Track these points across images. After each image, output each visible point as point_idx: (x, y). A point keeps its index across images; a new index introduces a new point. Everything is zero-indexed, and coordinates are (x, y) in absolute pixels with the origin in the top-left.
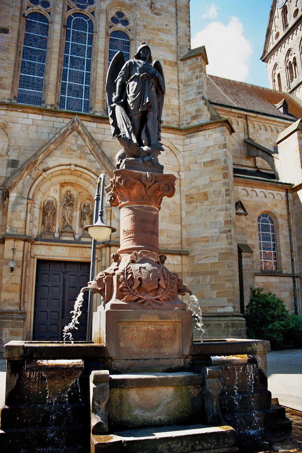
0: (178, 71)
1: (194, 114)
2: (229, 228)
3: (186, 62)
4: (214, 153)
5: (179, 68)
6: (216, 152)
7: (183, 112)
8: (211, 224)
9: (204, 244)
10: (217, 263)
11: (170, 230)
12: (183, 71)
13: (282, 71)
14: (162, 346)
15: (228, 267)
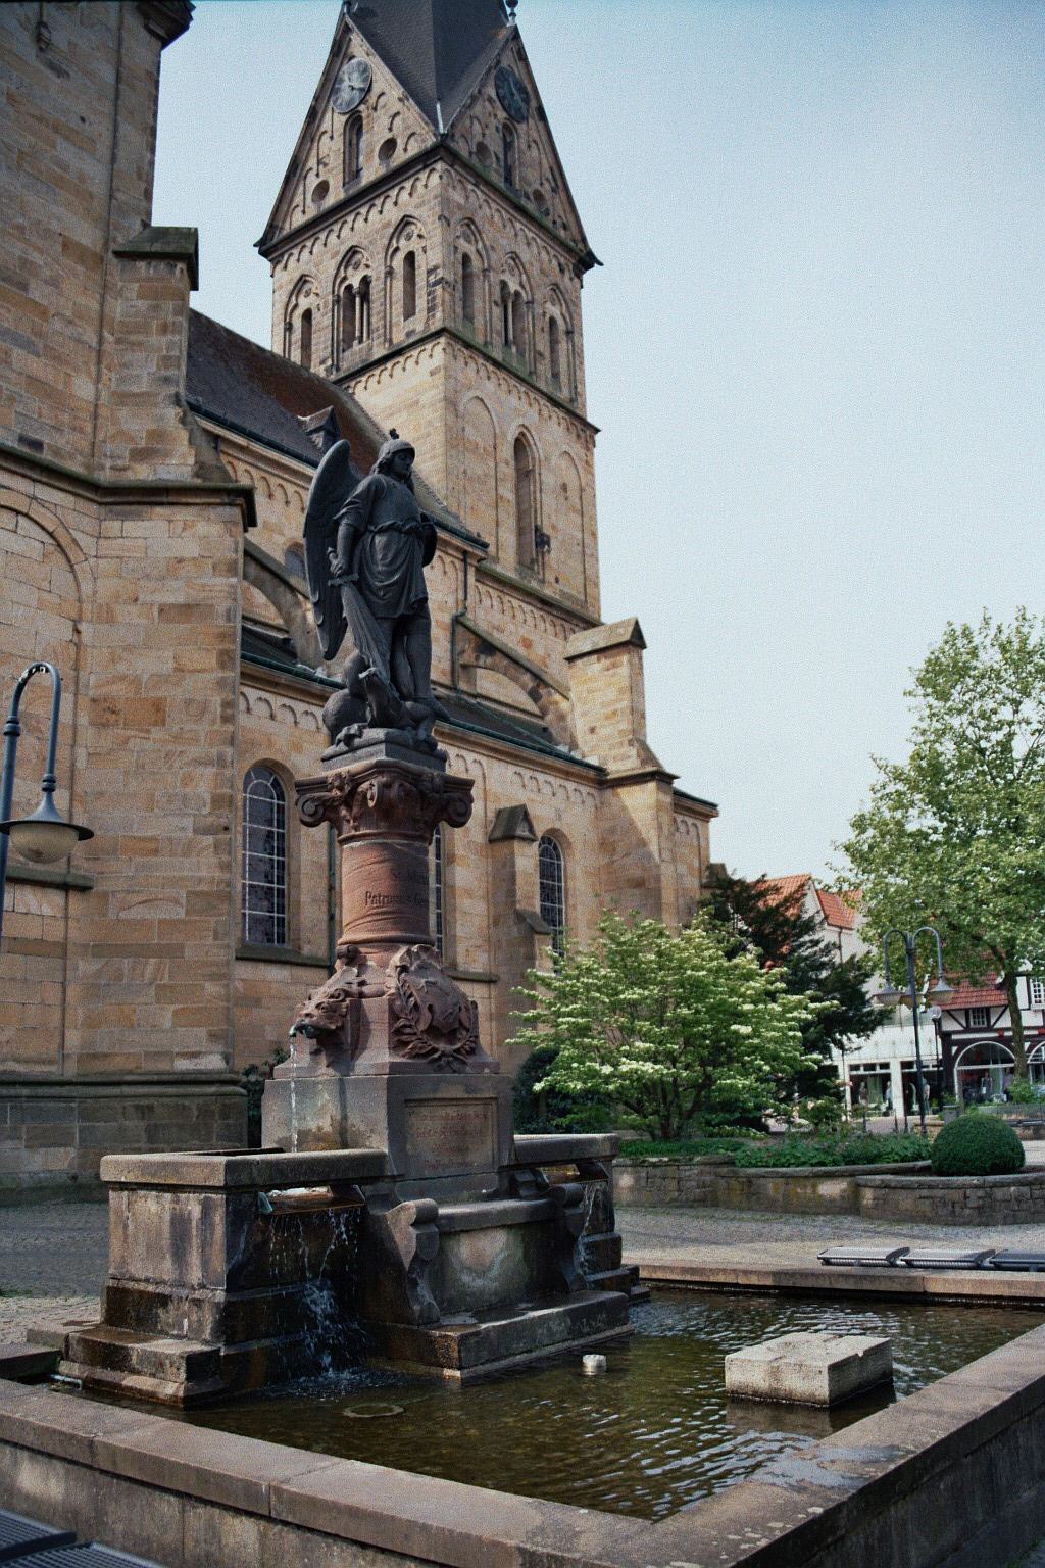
0: (105, 286)
1: (142, 444)
2: (224, 821)
3: (132, 263)
4: (198, 581)
5: (109, 277)
6: (205, 580)
7: (106, 430)
8: (170, 802)
9: (139, 859)
10: (179, 921)
12: (120, 293)
13: (322, 307)
15: (216, 938)
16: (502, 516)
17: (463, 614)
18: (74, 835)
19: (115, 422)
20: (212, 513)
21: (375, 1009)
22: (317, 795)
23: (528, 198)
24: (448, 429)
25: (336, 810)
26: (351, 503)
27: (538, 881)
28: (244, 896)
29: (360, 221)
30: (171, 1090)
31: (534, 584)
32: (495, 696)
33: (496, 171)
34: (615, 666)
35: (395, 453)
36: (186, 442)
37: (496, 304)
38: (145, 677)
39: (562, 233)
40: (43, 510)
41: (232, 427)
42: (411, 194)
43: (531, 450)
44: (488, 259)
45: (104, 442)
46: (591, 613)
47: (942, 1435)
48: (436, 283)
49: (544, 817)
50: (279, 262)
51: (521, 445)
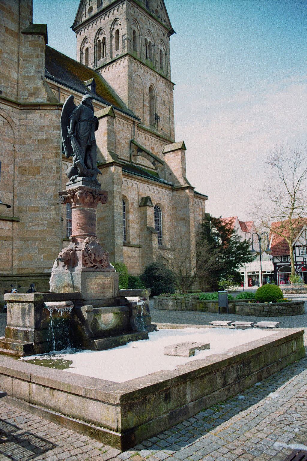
1: (32, 91)
6: (51, 132)
7: (21, 87)
8: (42, 196)
11: (3, 197)
13: (91, 47)
14: (105, 292)
16: (145, 110)
17: (133, 140)
18: (5, 207)
19: (24, 85)
20: (52, 112)
21: (79, 254)
22: (64, 196)
23: (153, 12)
24: (129, 84)
25: (70, 200)
26: (74, 113)
27: (154, 218)
28: (67, 223)
29: (102, 20)
30: (43, 278)
31: (155, 131)
32: (143, 164)
33: (143, 3)
34: (177, 155)
35: (86, 99)
36: (45, 91)
37: (144, 46)
38: (34, 161)
39: (164, 23)
40: (3, 112)
41: (63, 85)
42: (117, 11)
43: (154, 91)
44: (141, 32)
45: (21, 91)
46: (172, 139)
47: (206, 365)
48: (125, 40)
49: (155, 199)
50: (78, 33)
51: (151, 89)
